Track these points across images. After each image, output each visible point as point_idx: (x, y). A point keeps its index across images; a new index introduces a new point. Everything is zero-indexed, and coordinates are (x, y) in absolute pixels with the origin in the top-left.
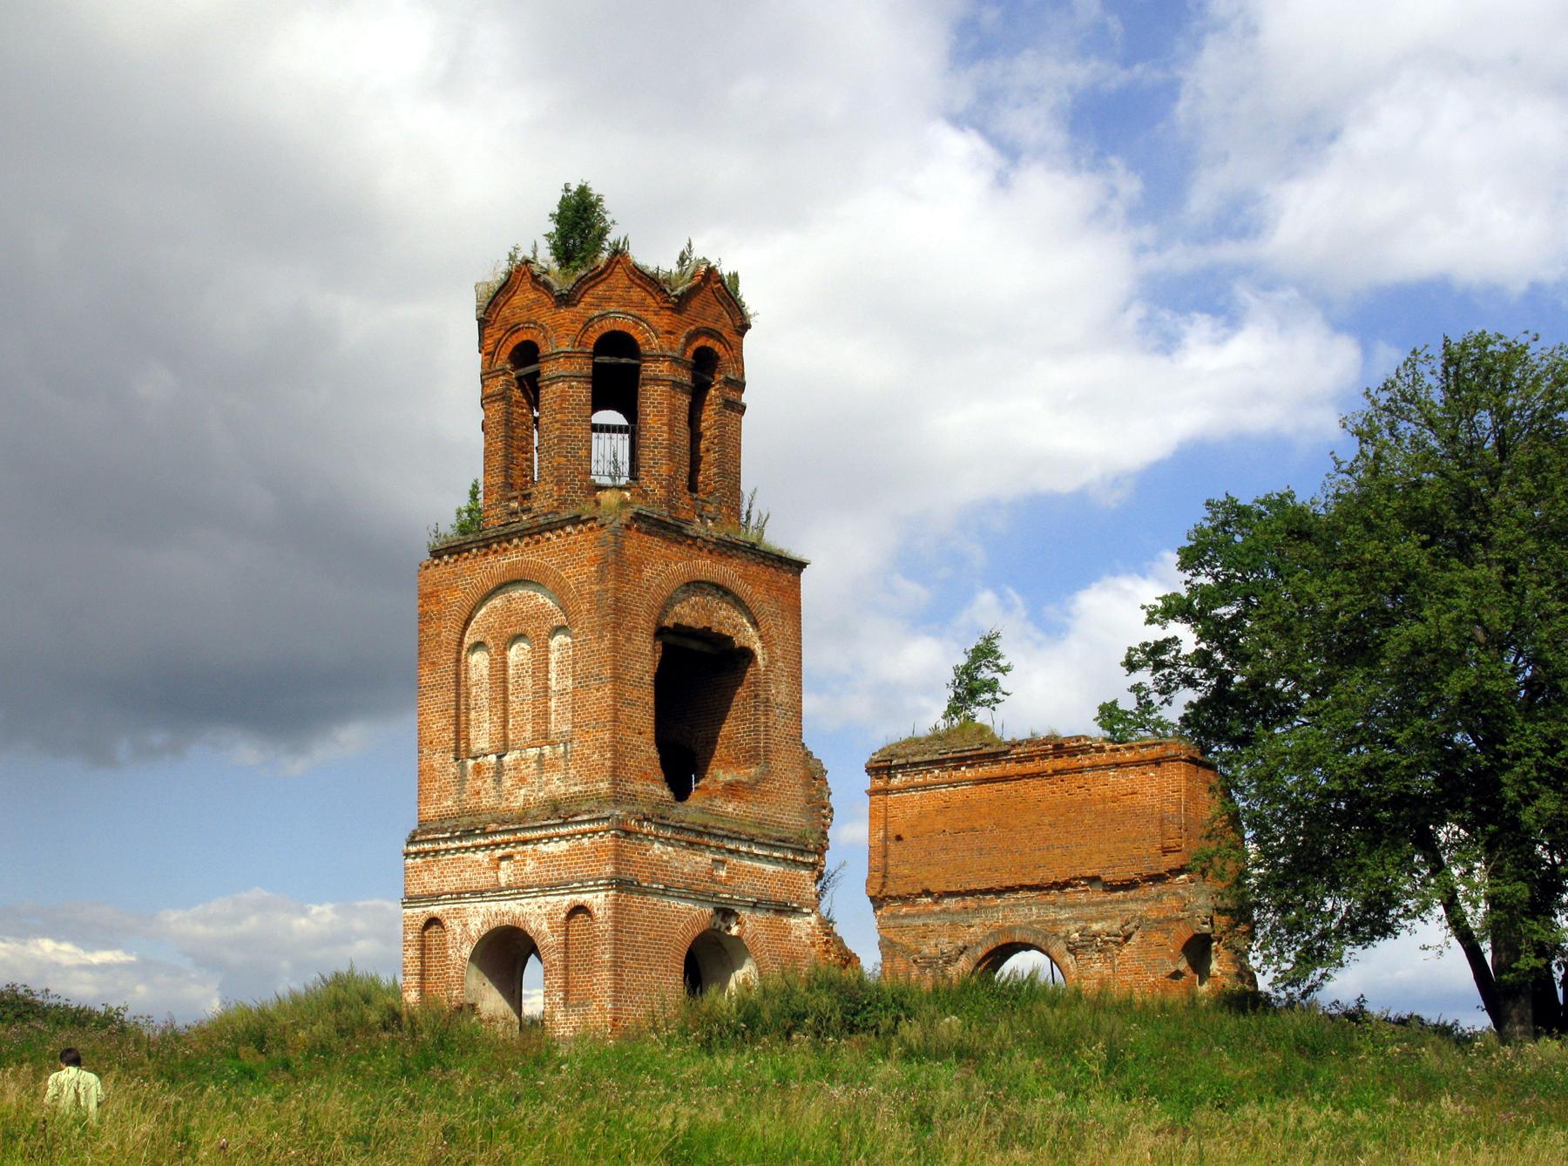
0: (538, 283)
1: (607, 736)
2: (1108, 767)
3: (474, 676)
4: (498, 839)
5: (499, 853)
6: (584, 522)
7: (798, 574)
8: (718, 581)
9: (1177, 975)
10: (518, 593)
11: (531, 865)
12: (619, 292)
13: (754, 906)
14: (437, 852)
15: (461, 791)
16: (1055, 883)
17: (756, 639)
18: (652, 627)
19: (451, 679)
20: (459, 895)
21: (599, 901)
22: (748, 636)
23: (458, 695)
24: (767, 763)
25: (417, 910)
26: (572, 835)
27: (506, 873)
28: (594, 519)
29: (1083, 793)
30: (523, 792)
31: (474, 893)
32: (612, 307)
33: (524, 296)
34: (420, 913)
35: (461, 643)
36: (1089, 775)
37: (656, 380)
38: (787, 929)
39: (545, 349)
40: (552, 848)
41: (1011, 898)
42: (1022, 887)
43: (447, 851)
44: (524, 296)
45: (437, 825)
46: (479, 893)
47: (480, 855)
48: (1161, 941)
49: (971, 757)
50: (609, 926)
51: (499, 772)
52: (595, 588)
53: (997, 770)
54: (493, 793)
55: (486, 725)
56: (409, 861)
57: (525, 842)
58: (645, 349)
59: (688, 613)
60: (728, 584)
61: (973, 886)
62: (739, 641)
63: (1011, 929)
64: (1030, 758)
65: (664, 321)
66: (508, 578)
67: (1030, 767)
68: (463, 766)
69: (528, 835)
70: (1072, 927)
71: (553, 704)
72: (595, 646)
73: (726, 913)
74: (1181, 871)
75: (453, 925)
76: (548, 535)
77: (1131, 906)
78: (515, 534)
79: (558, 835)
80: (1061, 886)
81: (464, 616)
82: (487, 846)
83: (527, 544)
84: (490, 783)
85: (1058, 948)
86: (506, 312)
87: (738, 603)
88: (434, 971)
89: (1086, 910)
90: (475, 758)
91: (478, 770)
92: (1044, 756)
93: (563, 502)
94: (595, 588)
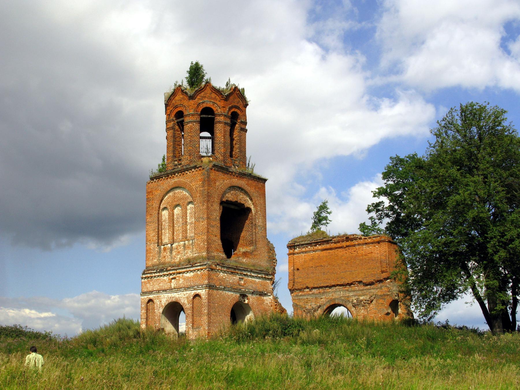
1: (205, 237)
2: (363, 244)
3: (163, 218)
4: (171, 272)
5: (171, 277)
7: (264, 183)
9: (388, 314)
10: (177, 191)
11: (181, 281)
12: (208, 95)
13: (253, 293)
14: (152, 277)
15: (159, 257)
16: (348, 284)
17: (252, 204)
20: (158, 291)
21: (203, 292)
23: (158, 225)
24: (256, 244)
25: (145, 297)
26: (195, 271)
27: (173, 284)
28: (201, 167)
30: (179, 256)
32: (206, 100)
34: (146, 298)
35: (159, 208)
36: (357, 247)
37: (220, 122)
38: (263, 301)
39: (186, 113)
41: (334, 289)
42: (338, 285)
43: (155, 276)
45: (152, 268)
46: (165, 291)
47: (165, 278)
48: (382, 302)
49: (320, 242)
50: (206, 301)
51: (171, 250)
52: (201, 189)
53: (328, 246)
55: (167, 234)
56: (143, 280)
57: (180, 273)
58: (216, 112)
59: (230, 196)
60: (242, 187)
61: (322, 285)
62: (246, 205)
63: (334, 299)
64: (339, 242)
65: (222, 103)
67: (339, 245)
68: (160, 248)
70: (354, 298)
71: (188, 227)
72: (201, 208)
73: (244, 296)
74: (388, 278)
75: (157, 301)
76: (186, 172)
77: (372, 291)
78: (176, 172)
80: (350, 284)
81: (161, 199)
82: (168, 275)
83: (180, 175)
86: (174, 102)
87: (246, 193)
91: (165, 249)
92: (343, 241)
93: (191, 161)
94: (201, 189)
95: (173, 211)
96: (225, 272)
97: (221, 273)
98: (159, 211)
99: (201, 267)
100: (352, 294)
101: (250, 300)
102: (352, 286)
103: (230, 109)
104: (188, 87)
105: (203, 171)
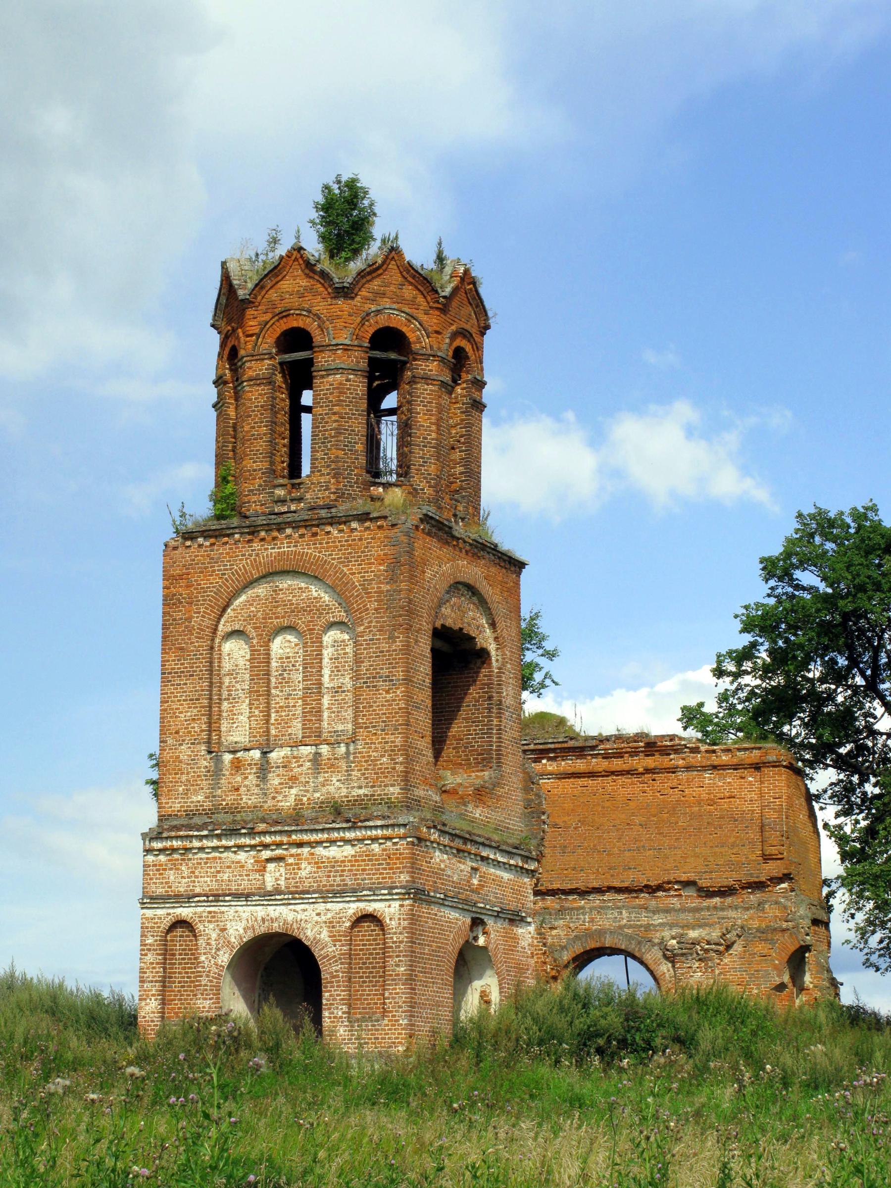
0: (314, 272)
1: (399, 741)
2: (704, 768)
3: (227, 666)
4: (268, 839)
5: (266, 854)
6: (371, 520)
7: (519, 574)
8: (471, 582)
9: (781, 987)
10: (286, 583)
11: (306, 870)
12: (392, 288)
13: (497, 916)
14: (187, 850)
15: (215, 786)
16: (646, 886)
17: (491, 640)
18: (430, 627)
19: (203, 665)
20: (216, 897)
21: (391, 910)
22: (486, 639)
24: (499, 764)
25: (160, 912)
26: (361, 840)
27: (274, 876)
28: (385, 517)
29: (675, 795)
30: (294, 791)
31: (237, 896)
32: (386, 303)
33: (294, 283)
34: (165, 914)
35: (215, 630)
36: (683, 776)
37: (427, 379)
38: (516, 938)
39: (317, 339)
40: (333, 852)
41: (595, 900)
42: (610, 889)
43: (201, 849)
44: (294, 283)
45: (183, 821)
46: (245, 896)
47: (242, 856)
48: (765, 952)
49: (553, 750)
50: (404, 937)
51: (264, 769)
52: (385, 587)
53: (580, 765)
54: (256, 790)
55: (243, 719)
56: (150, 858)
57: (300, 845)
58: (416, 347)
59: (450, 617)
60: (477, 585)
61: (555, 886)
62: (480, 642)
63: (601, 933)
64: (619, 755)
65: (433, 320)
66: (278, 567)
67: (617, 764)
68: (218, 760)
69: (306, 837)
70: (667, 934)
71: (326, 701)
72: (385, 646)
73: (477, 922)
74: (781, 880)
75: (208, 931)
76: (329, 528)
77: (731, 914)
78: (289, 524)
79: (343, 840)
80: (651, 890)
81: (221, 603)
82: (253, 847)
84: (252, 779)
85: (653, 955)
86: (273, 295)
87: (483, 603)
88: (177, 978)
89: (682, 916)
90: (234, 752)
91: (237, 766)
92: (634, 753)
93: (341, 495)
94: (385, 587)
95: (267, 645)
96: (444, 848)
97: (437, 853)
98: (213, 640)
99: (388, 832)
100: (663, 922)
101: (490, 937)
102: (660, 894)
103: (454, 336)
104: (325, 257)
105: (391, 533)
